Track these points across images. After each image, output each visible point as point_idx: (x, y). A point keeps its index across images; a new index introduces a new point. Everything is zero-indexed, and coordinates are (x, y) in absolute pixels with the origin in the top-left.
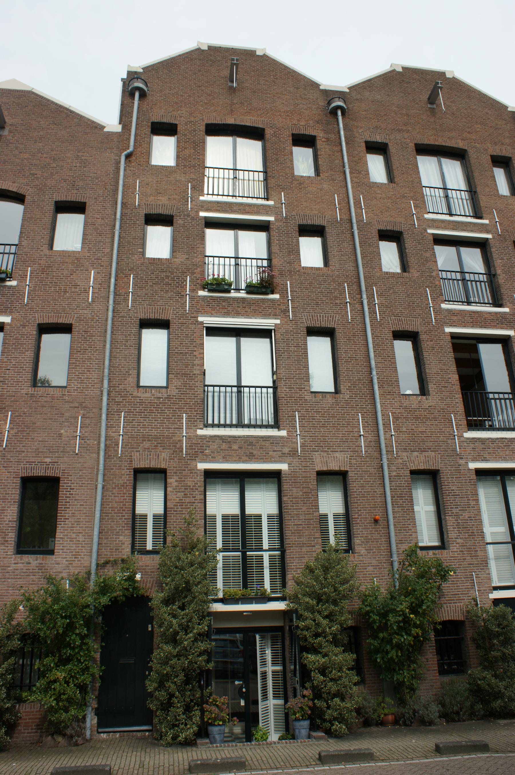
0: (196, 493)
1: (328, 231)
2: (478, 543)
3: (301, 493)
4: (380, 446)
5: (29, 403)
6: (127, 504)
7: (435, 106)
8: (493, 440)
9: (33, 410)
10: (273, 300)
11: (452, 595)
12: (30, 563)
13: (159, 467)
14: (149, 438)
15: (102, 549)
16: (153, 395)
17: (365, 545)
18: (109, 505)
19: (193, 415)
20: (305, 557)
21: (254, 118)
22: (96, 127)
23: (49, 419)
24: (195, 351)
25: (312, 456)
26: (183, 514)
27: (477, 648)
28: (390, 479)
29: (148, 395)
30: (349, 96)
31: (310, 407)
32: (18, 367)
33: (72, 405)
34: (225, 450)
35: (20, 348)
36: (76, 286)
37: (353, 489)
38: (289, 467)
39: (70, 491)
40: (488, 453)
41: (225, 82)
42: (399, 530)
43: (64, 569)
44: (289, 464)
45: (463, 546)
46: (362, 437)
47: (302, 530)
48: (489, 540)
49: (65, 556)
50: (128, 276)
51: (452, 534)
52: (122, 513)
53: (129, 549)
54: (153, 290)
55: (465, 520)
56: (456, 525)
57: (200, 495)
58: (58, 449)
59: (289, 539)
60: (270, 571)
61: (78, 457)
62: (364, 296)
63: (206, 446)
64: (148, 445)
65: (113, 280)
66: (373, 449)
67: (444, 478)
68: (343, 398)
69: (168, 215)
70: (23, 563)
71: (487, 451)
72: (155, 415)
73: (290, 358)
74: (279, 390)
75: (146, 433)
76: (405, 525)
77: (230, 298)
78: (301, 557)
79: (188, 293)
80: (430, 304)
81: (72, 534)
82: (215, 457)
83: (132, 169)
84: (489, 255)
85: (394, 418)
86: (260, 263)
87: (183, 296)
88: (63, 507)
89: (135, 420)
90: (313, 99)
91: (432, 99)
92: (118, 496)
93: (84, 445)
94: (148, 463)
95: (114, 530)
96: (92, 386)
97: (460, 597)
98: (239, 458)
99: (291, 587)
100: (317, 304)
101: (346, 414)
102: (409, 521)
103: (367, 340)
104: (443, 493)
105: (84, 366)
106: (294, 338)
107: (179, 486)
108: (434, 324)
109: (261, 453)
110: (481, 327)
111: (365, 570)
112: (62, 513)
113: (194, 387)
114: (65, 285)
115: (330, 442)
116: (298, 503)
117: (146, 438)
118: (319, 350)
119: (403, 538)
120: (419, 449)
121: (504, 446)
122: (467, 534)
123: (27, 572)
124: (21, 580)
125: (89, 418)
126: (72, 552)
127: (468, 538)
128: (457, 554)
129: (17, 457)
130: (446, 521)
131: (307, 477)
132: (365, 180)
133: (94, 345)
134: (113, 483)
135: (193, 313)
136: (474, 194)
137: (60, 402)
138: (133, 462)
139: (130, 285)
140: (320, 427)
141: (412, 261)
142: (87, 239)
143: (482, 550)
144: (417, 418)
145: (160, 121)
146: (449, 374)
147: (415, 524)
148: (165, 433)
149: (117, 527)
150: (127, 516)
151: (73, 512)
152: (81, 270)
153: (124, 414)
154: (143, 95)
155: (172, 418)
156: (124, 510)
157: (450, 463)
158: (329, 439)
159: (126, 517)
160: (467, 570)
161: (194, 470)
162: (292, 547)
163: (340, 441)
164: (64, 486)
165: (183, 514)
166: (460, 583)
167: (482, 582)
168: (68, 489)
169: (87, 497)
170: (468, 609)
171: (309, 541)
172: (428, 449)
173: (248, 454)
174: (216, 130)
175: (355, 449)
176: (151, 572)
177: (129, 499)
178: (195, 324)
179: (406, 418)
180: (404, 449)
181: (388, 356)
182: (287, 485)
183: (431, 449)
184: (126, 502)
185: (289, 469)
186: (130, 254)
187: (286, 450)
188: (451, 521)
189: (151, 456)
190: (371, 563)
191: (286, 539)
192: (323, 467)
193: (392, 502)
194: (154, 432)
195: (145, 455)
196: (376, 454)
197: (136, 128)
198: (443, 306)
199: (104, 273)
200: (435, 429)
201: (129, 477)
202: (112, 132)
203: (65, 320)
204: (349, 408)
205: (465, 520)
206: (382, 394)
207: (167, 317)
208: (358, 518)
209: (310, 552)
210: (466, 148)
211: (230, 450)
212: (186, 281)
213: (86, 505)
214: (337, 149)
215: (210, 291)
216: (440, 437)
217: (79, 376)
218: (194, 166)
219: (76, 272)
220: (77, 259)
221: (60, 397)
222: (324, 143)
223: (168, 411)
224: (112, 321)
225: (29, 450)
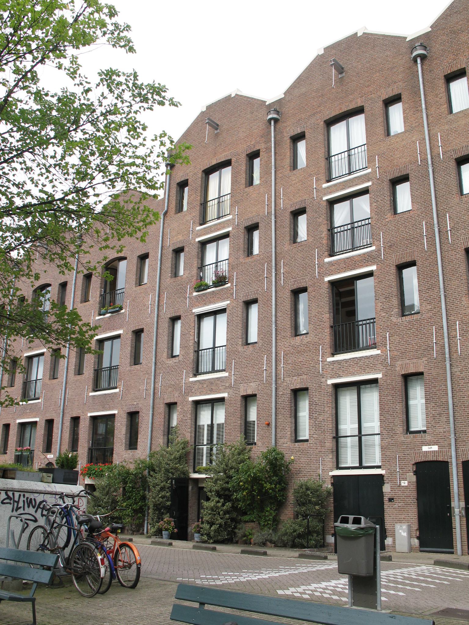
7: (344, 74)
8: (346, 361)
144: (299, 352)
187: (227, 385)
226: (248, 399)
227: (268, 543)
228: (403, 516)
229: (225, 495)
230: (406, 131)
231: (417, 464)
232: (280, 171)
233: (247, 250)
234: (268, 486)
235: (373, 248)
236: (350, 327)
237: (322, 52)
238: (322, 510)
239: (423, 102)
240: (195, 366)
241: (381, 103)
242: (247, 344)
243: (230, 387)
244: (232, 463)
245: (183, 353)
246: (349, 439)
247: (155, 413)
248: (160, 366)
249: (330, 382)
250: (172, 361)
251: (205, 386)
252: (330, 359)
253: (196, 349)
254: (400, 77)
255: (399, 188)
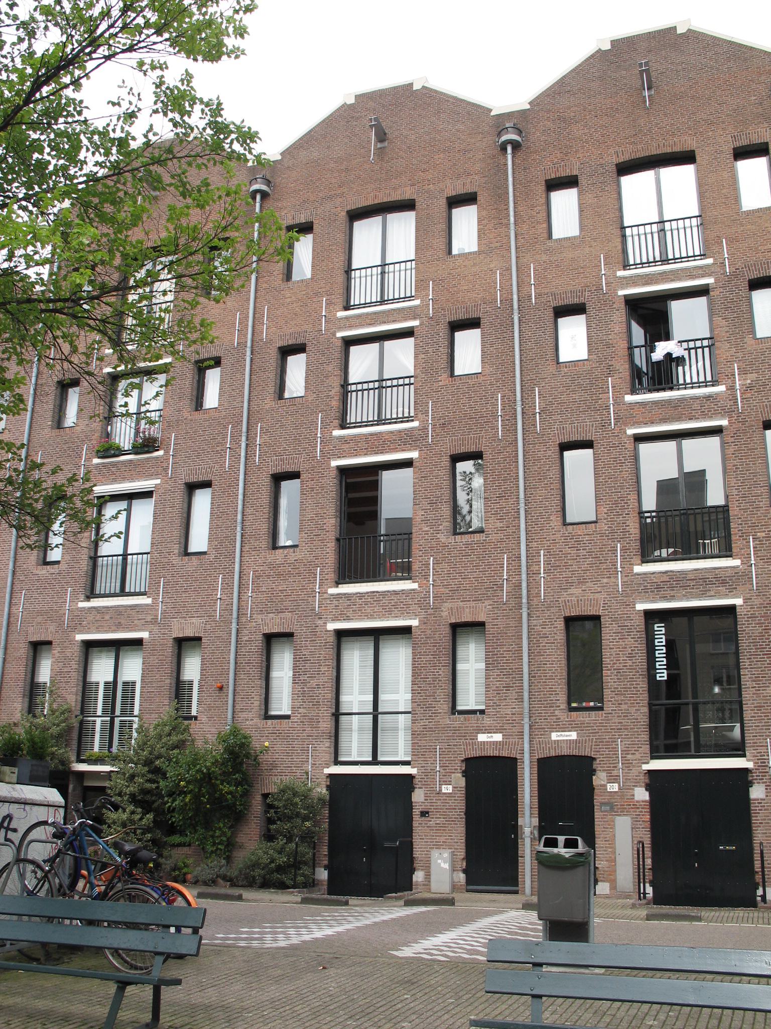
7: (386, 144)
8: (361, 595)
117: (40, 613)
144: (279, 575)
161: (72, 641)
187: (149, 618)
226: (183, 644)
227: (220, 881)
228: (442, 839)
229: (144, 801)
230: (479, 253)
231: (468, 761)
232: (264, 279)
233: (195, 399)
234: (226, 788)
235: (416, 424)
236: (356, 544)
237: (351, 101)
238: (313, 828)
239: (512, 213)
240: (89, 583)
241: (445, 201)
242: (187, 554)
243: (154, 621)
244: (159, 748)
245: (67, 557)
246: (355, 718)
247: (9, 659)
248: (22, 578)
249: (332, 626)
250: (44, 571)
251: (107, 617)
252: (332, 591)
253: (92, 554)
254: (478, 167)
255: (292, 360)
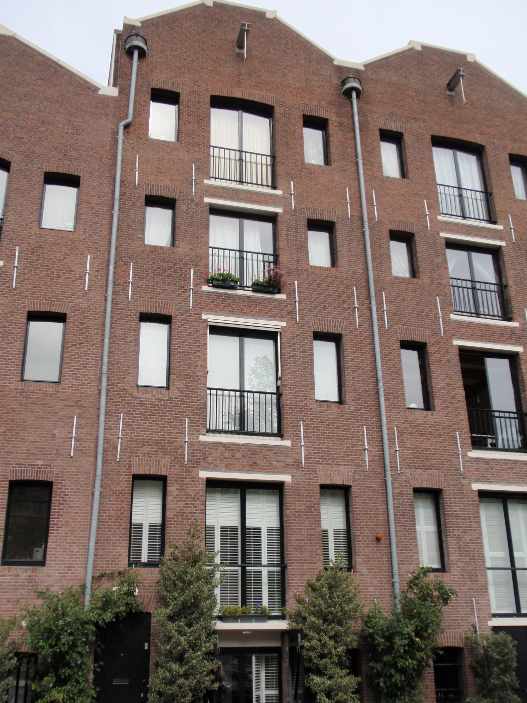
0: (198, 502)
1: (338, 228)
2: (479, 567)
3: (304, 507)
4: (384, 462)
5: (18, 399)
6: (125, 512)
7: (453, 93)
8: (497, 462)
9: (24, 407)
10: (279, 301)
11: (452, 620)
12: (18, 576)
13: (159, 474)
14: (149, 442)
15: (97, 561)
16: (154, 396)
17: (367, 564)
18: (105, 513)
19: (195, 420)
20: (306, 574)
21: (262, 93)
22: (90, 89)
23: (42, 418)
24: (199, 351)
25: (316, 469)
26: (184, 524)
27: (475, 676)
28: (393, 496)
29: (149, 396)
30: (364, 75)
31: (315, 417)
32: (6, 359)
33: (66, 403)
34: (228, 458)
35: (8, 338)
36: (70, 271)
37: (356, 505)
38: (292, 479)
39: (64, 498)
40: (492, 474)
41: (232, 48)
42: (401, 550)
43: (56, 583)
44: (292, 476)
45: (463, 570)
46: (366, 450)
47: (304, 546)
48: (488, 565)
49: (57, 568)
50: (127, 264)
51: (453, 556)
52: (120, 522)
53: (126, 562)
54: (154, 282)
55: (466, 543)
56: (458, 548)
57: (201, 505)
58: (51, 451)
59: (291, 554)
60: (269, 588)
61: (73, 461)
62: (373, 302)
63: (209, 454)
64: (148, 449)
65: (112, 268)
66: (376, 464)
67: (446, 498)
68: (348, 409)
69: (170, 198)
70: (11, 575)
71: (491, 472)
72: (156, 418)
73: (295, 364)
74: (284, 397)
75: (146, 436)
76: (406, 545)
77: (235, 295)
78: (303, 574)
79: (192, 287)
80: (439, 314)
81: (65, 544)
82: (217, 466)
83: (131, 141)
84: (501, 263)
85: (398, 432)
86: (266, 258)
87: (186, 290)
88: (56, 514)
89: (134, 422)
90: (326, 76)
91: (452, 85)
92: (116, 504)
93: (79, 447)
94: (147, 469)
95: (110, 540)
96: (88, 383)
97: (460, 623)
98: (242, 467)
99: (292, 606)
100: (325, 307)
101: (351, 426)
102: (411, 541)
103: (374, 349)
104: (445, 514)
105: (80, 361)
106: (300, 342)
107: (179, 495)
108: (442, 335)
109: (264, 463)
110: (490, 341)
111: (366, 591)
112: (54, 521)
113: (197, 389)
114: (58, 270)
115: (335, 454)
116: (300, 518)
117: (145, 442)
118: (324, 355)
119: (404, 558)
120: (422, 466)
121: (508, 468)
122: (468, 558)
123: (15, 586)
124: (8, 594)
125: (85, 418)
126: (65, 564)
127: (469, 562)
128: (458, 578)
129: (5, 458)
130: (447, 543)
131: (310, 490)
132: (378, 174)
133: (91, 339)
134: (110, 490)
135: (197, 310)
136: (490, 196)
137: (53, 399)
138: (132, 468)
139: (129, 274)
140: (324, 438)
141: (423, 265)
142: (82, 219)
143: (482, 575)
144: (421, 434)
145: (161, 88)
146: (456, 389)
147: (416, 545)
148: (167, 438)
149: (114, 537)
150: (125, 525)
151: (67, 520)
152: (75, 254)
153: (123, 416)
154: (142, 54)
155: (173, 422)
156: (122, 519)
157: (453, 482)
158: (333, 451)
159: (124, 527)
160: (467, 595)
161: (195, 479)
162: (294, 563)
163: (344, 455)
164: (57, 492)
165: (184, 524)
166: (460, 609)
167: (481, 609)
168: (61, 495)
169: (82, 504)
170: (467, 636)
171: (310, 557)
172: (432, 467)
173: (251, 463)
174: (220, 102)
175: (359, 463)
176: (149, 586)
177: (127, 507)
178: (199, 322)
179: (411, 434)
180: (408, 465)
181: (395, 367)
182: (290, 498)
183: (434, 467)
184: (124, 511)
185: (292, 481)
186: (129, 239)
187: (290, 461)
188: (452, 543)
189: (152, 462)
190: (372, 583)
191: (288, 554)
192: (326, 479)
193: (395, 520)
194: (155, 437)
195: (145, 461)
196: (379, 470)
197: (136, 94)
198: (453, 317)
199: (101, 259)
200: (440, 447)
201: (128, 484)
202: (107, 96)
203: (58, 309)
204: (354, 419)
205: (466, 543)
206: (388, 407)
207: (169, 312)
208: (360, 536)
209: (312, 569)
210: (484, 144)
211: (233, 459)
212: (190, 274)
213: (81, 513)
214: (350, 135)
215: (214, 286)
216: (444, 455)
217: (74, 371)
218: (198, 144)
219: (69, 256)
220: (71, 240)
221: (54, 394)
222: (337, 128)
223: (169, 414)
224: (112, 313)
225: (19, 451)
251: (238, 455)
